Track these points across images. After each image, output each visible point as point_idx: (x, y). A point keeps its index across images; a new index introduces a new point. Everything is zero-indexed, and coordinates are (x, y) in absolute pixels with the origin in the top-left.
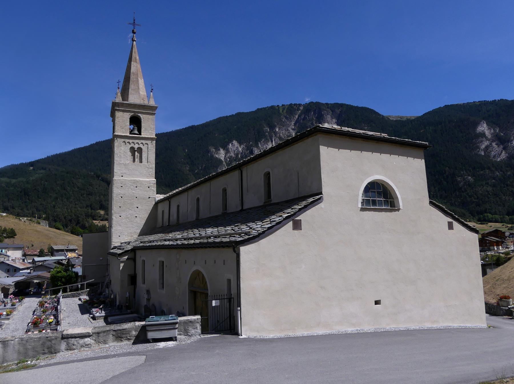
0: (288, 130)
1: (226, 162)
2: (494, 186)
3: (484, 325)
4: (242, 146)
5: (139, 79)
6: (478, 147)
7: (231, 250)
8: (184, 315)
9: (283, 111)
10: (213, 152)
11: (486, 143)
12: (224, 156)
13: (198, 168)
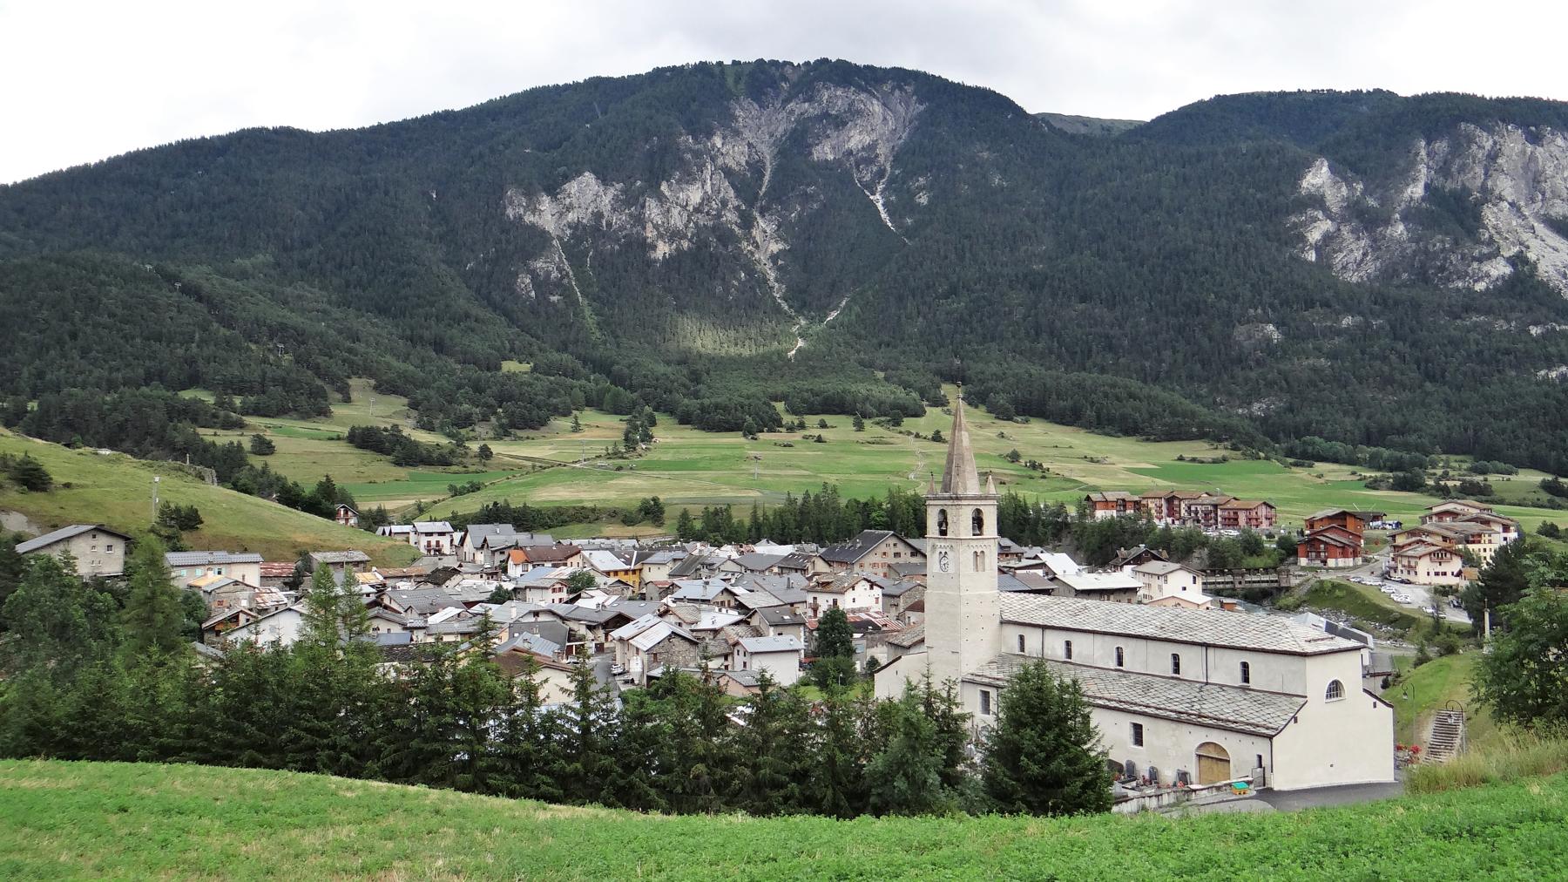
2: (1333, 356)
3: (1391, 779)
6: (1302, 238)
11: (1326, 226)
13: (477, 257)
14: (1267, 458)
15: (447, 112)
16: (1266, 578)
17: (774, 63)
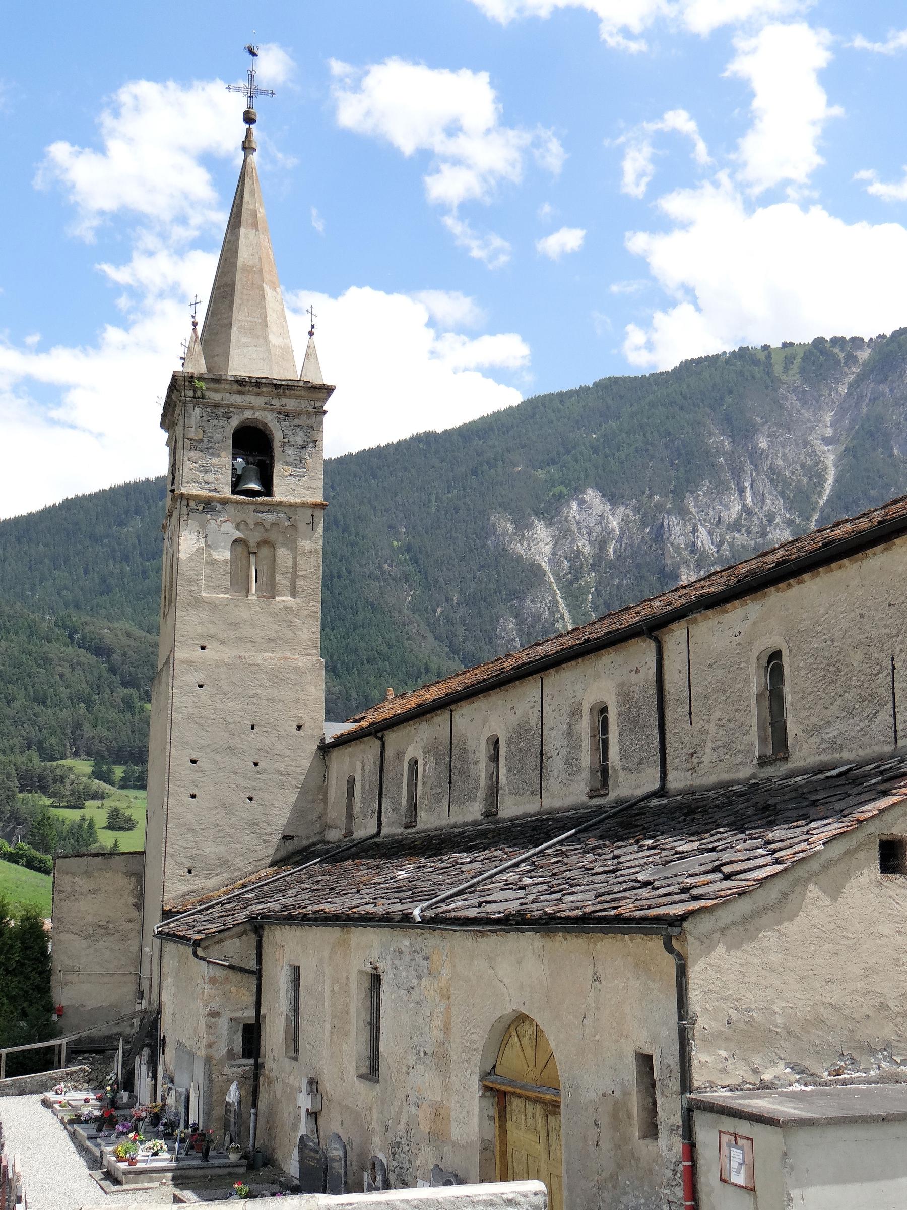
0: (806, 443)
4: (621, 510)
7: (655, 944)
8: (461, 1181)
9: (786, 369)
10: (506, 533)
12: (548, 549)
13: (448, 600)
16: (579, 897)
17: (837, 341)
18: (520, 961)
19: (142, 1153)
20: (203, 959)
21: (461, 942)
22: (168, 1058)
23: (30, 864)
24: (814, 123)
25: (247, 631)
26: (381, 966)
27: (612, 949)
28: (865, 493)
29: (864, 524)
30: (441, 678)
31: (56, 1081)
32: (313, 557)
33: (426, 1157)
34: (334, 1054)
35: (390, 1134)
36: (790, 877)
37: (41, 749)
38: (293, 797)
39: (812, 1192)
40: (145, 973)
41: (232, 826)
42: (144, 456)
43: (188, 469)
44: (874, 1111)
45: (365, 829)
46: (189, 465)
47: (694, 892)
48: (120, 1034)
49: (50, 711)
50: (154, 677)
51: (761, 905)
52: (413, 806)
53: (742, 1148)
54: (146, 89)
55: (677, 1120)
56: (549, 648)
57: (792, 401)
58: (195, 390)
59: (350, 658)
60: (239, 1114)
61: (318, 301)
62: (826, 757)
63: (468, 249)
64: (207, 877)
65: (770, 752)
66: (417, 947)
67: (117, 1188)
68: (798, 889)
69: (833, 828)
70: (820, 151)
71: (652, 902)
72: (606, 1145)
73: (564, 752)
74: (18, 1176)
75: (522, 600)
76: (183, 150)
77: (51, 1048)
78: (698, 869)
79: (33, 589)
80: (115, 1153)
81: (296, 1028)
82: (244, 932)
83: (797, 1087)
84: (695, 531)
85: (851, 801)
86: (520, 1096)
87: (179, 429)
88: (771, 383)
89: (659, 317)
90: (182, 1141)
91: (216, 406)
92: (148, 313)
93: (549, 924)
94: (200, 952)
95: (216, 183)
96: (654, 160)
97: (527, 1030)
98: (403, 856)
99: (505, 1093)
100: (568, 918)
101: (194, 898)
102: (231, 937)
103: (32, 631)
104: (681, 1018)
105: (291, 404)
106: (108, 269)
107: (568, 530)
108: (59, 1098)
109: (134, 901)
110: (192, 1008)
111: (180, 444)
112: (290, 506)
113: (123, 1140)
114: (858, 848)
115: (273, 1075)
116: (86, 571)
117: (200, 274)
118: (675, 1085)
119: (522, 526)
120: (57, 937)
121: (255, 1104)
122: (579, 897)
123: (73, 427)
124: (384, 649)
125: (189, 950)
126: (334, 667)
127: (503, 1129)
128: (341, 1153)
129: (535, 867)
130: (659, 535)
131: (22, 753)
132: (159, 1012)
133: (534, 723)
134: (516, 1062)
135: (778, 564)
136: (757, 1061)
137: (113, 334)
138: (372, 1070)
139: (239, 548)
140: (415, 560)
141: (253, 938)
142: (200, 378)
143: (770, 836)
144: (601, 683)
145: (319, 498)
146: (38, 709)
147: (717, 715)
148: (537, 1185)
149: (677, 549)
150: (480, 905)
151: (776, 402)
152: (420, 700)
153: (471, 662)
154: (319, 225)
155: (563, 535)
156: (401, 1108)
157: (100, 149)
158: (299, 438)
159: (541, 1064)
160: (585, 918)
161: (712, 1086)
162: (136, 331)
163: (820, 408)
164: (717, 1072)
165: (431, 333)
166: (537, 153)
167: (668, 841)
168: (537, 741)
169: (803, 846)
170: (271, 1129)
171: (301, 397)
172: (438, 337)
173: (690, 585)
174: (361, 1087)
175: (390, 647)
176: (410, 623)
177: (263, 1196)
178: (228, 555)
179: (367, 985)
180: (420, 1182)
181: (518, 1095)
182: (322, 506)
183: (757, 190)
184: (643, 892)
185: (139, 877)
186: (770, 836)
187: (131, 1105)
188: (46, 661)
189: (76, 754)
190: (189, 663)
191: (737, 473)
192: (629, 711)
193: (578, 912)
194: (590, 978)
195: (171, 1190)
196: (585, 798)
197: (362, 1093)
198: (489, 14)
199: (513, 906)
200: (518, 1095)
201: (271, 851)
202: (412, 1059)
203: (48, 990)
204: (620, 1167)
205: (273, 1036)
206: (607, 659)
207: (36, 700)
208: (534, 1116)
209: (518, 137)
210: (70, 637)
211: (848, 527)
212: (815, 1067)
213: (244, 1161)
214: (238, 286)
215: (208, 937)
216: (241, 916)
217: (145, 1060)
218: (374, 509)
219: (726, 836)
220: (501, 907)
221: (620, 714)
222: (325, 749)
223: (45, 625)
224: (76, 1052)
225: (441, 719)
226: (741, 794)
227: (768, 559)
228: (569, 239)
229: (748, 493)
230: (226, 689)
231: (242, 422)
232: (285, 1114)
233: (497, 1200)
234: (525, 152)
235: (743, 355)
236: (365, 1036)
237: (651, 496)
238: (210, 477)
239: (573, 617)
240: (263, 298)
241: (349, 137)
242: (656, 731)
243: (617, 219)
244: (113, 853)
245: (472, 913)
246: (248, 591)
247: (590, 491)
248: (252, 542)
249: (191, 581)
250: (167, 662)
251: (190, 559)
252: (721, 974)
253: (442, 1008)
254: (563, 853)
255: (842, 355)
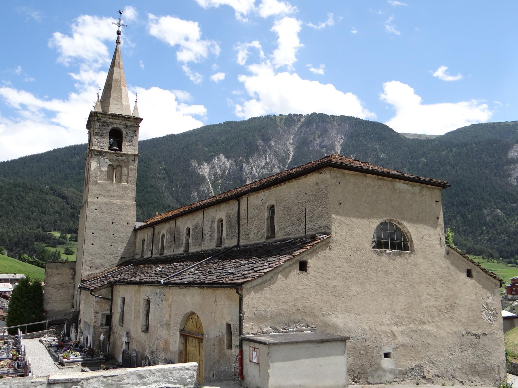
0: (285, 144)
1: (210, 180)
4: (230, 161)
5: (122, 87)
7: (234, 291)
8: (173, 363)
9: (280, 122)
10: (195, 166)
12: (208, 172)
13: (177, 186)
14: (498, 262)
15: (172, 135)
16: (212, 277)
17: (295, 115)
18: (193, 296)
19: (72, 356)
20: (94, 295)
21: (175, 290)
22: (82, 326)
23: (38, 265)
24: (295, 48)
25: (112, 193)
26: (150, 297)
27: (221, 293)
28: (301, 160)
29: (300, 169)
30: (174, 209)
31: (44, 334)
32: (134, 171)
33: (162, 356)
34: (135, 325)
35: (151, 349)
36: (274, 272)
37: (43, 229)
38: (125, 245)
39: (276, 364)
40: (75, 299)
41: (105, 254)
42: (80, 136)
43: (95, 141)
44: (294, 340)
45: (147, 255)
46: (95, 140)
47: (246, 276)
48: (66, 319)
49: (46, 217)
50: (82, 207)
51: (265, 280)
52: (162, 248)
53: (256, 351)
54: (87, 18)
55: (238, 343)
56: (206, 202)
57: (281, 132)
58: (98, 117)
59: (145, 201)
60: (104, 343)
61: (140, 90)
62: (286, 237)
63: (189, 77)
64: (96, 270)
65: (270, 235)
66: (162, 292)
67: (63, 367)
68: (276, 276)
69: (286, 258)
70: (297, 56)
71: (233, 279)
72: (217, 351)
73: (209, 233)
74: (30, 365)
75: (200, 186)
76: (99, 39)
77: (43, 323)
78: (247, 269)
79: (42, 177)
80: (63, 356)
81: (123, 316)
82: (108, 287)
83: (273, 333)
84: (252, 168)
85: (292, 250)
86: (191, 337)
87: (92, 129)
88: (276, 126)
89: (246, 103)
90: (85, 352)
91: (105, 122)
92: (85, 90)
93: (202, 285)
94: (93, 293)
95: (109, 50)
96: (247, 54)
97: (194, 317)
98: (159, 264)
99: (187, 336)
100: (208, 283)
101: (92, 276)
102: (103, 288)
103: (41, 191)
104: (240, 313)
105: (129, 123)
106: (73, 75)
107: (214, 166)
108: (45, 339)
109: (71, 277)
110: (89, 310)
111: (92, 133)
112: (127, 155)
113: (66, 352)
114: (294, 264)
115: (115, 331)
116: (60, 172)
117: (102, 79)
118: (237, 333)
119: (200, 164)
120: (46, 288)
121: (109, 340)
122: (212, 277)
123: (58, 125)
124: (156, 200)
125: (89, 293)
126: (140, 204)
127: (186, 346)
128: (135, 355)
129: (199, 268)
130: (241, 169)
131: (36, 229)
132: (79, 312)
133: (201, 224)
134: (191, 326)
135: (274, 180)
136: (262, 326)
137: (74, 96)
138: (146, 329)
139: (110, 167)
140: (167, 173)
141: (110, 289)
142: (100, 113)
143: (269, 260)
144: (221, 213)
145: (137, 153)
146: (42, 215)
147: (255, 223)
148: (195, 364)
149: (246, 173)
150: (182, 279)
151: (277, 131)
152: (166, 216)
153: (183, 205)
154: (142, 66)
155: (212, 167)
156: (155, 341)
157: (71, 36)
158: (131, 134)
159: (198, 327)
160: (213, 283)
161: (248, 333)
162: (81, 95)
163: (289, 134)
164: (250, 329)
165: (176, 103)
166: (211, 48)
167: (239, 260)
168: (201, 230)
169: (278, 263)
170: (114, 348)
171: (132, 121)
172: (179, 104)
173: (249, 184)
174: (142, 334)
175: (158, 199)
176: (165, 192)
177: (110, 369)
178: (107, 169)
179: (146, 303)
180: (160, 363)
181: (191, 336)
182: (137, 155)
183: (277, 67)
184: (231, 276)
185: (74, 269)
186: (269, 260)
187: (69, 341)
188: (45, 200)
189: (55, 230)
190: (93, 202)
191: (265, 152)
192: (229, 221)
193: (211, 281)
194: (214, 301)
195: (81, 367)
196: (215, 247)
197: (143, 336)
198: (200, 4)
199: (192, 279)
200: (191, 336)
201: (117, 262)
202: (159, 326)
203: (43, 305)
204: (220, 357)
205: (116, 319)
206: (223, 206)
207: (42, 213)
208: (196, 342)
209: (206, 43)
210: (54, 193)
211: (295, 170)
212: (278, 328)
213: (105, 358)
214: (113, 85)
215: (96, 288)
216: (107, 282)
217: (74, 327)
218: (155, 157)
219: (255, 259)
220: (188, 280)
221: (226, 222)
222: (136, 230)
223: (46, 189)
224: (51, 325)
225: (172, 223)
226: (261, 247)
227: (272, 178)
228: (220, 76)
229: (268, 158)
230: (104, 211)
231: (112, 127)
232: (119, 343)
233: (183, 368)
234: (208, 48)
235: (268, 117)
236: (144, 319)
237: (239, 157)
238: (102, 145)
239: (214, 192)
240: (121, 89)
241: (153, 38)
242: (237, 228)
243: (235, 71)
244: (66, 262)
245: (179, 281)
246: (113, 180)
247: (221, 155)
248: (115, 165)
249: (94, 177)
250: (85, 202)
251: (94, 170)
252: (252, 300)
253: (169, 310)
254: (208, 264)
255: (296, 119)
